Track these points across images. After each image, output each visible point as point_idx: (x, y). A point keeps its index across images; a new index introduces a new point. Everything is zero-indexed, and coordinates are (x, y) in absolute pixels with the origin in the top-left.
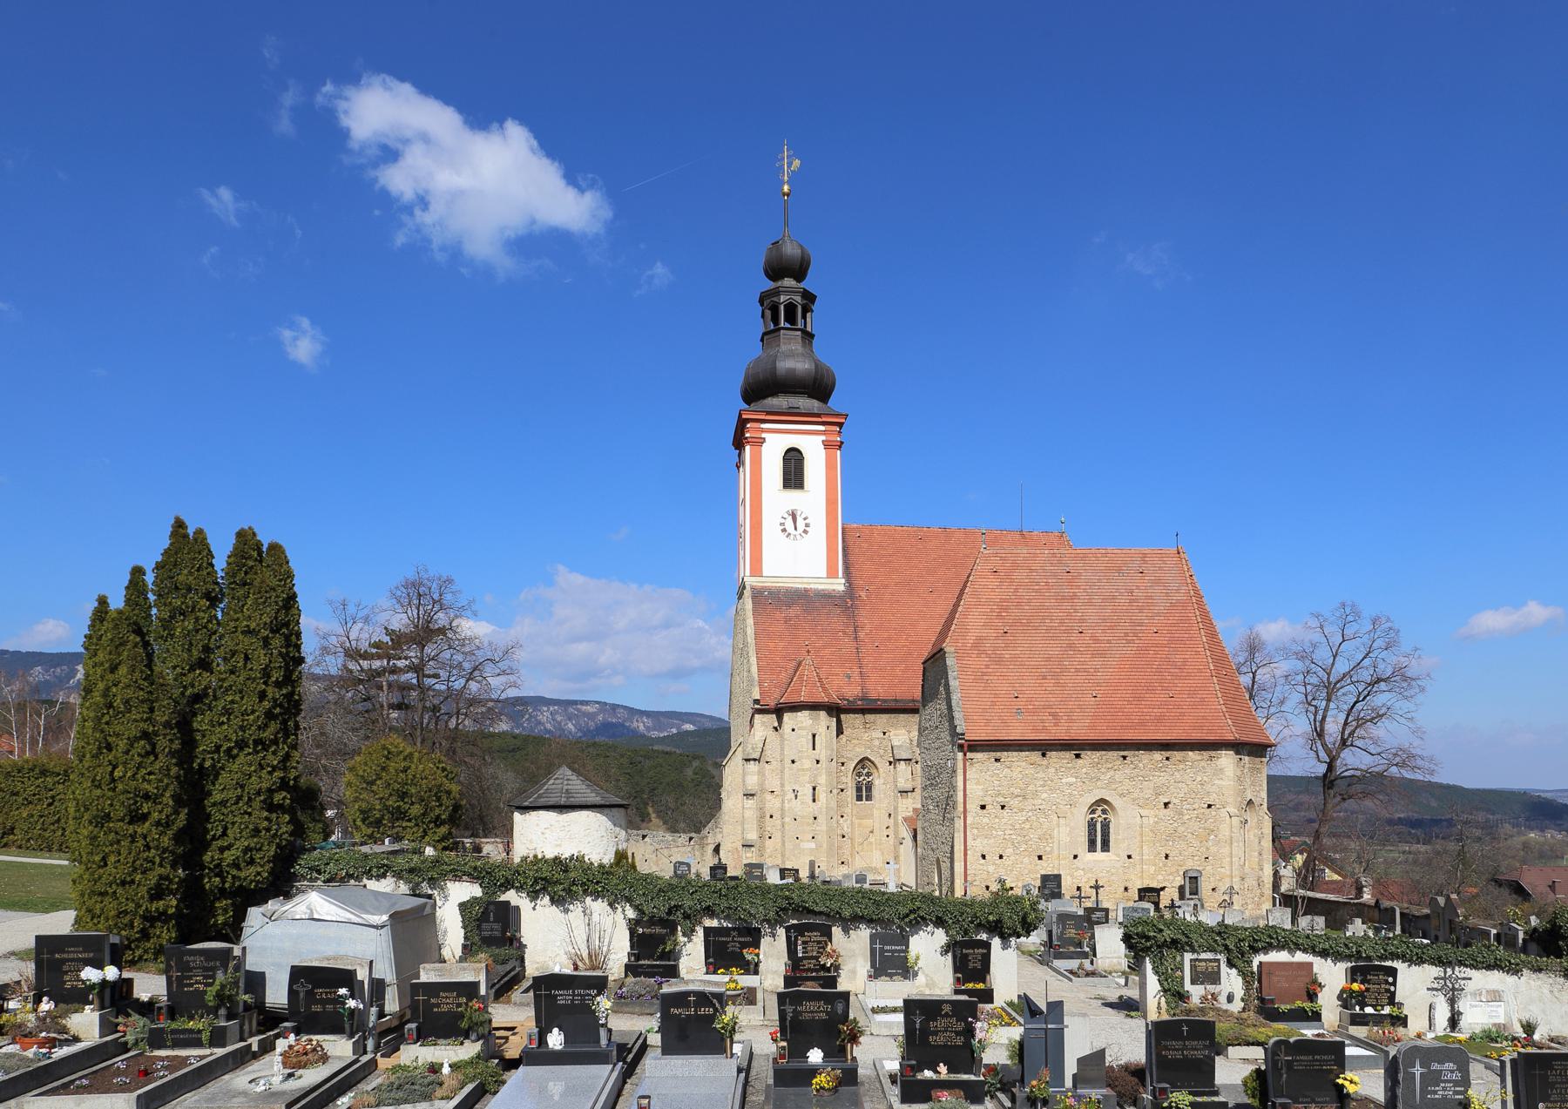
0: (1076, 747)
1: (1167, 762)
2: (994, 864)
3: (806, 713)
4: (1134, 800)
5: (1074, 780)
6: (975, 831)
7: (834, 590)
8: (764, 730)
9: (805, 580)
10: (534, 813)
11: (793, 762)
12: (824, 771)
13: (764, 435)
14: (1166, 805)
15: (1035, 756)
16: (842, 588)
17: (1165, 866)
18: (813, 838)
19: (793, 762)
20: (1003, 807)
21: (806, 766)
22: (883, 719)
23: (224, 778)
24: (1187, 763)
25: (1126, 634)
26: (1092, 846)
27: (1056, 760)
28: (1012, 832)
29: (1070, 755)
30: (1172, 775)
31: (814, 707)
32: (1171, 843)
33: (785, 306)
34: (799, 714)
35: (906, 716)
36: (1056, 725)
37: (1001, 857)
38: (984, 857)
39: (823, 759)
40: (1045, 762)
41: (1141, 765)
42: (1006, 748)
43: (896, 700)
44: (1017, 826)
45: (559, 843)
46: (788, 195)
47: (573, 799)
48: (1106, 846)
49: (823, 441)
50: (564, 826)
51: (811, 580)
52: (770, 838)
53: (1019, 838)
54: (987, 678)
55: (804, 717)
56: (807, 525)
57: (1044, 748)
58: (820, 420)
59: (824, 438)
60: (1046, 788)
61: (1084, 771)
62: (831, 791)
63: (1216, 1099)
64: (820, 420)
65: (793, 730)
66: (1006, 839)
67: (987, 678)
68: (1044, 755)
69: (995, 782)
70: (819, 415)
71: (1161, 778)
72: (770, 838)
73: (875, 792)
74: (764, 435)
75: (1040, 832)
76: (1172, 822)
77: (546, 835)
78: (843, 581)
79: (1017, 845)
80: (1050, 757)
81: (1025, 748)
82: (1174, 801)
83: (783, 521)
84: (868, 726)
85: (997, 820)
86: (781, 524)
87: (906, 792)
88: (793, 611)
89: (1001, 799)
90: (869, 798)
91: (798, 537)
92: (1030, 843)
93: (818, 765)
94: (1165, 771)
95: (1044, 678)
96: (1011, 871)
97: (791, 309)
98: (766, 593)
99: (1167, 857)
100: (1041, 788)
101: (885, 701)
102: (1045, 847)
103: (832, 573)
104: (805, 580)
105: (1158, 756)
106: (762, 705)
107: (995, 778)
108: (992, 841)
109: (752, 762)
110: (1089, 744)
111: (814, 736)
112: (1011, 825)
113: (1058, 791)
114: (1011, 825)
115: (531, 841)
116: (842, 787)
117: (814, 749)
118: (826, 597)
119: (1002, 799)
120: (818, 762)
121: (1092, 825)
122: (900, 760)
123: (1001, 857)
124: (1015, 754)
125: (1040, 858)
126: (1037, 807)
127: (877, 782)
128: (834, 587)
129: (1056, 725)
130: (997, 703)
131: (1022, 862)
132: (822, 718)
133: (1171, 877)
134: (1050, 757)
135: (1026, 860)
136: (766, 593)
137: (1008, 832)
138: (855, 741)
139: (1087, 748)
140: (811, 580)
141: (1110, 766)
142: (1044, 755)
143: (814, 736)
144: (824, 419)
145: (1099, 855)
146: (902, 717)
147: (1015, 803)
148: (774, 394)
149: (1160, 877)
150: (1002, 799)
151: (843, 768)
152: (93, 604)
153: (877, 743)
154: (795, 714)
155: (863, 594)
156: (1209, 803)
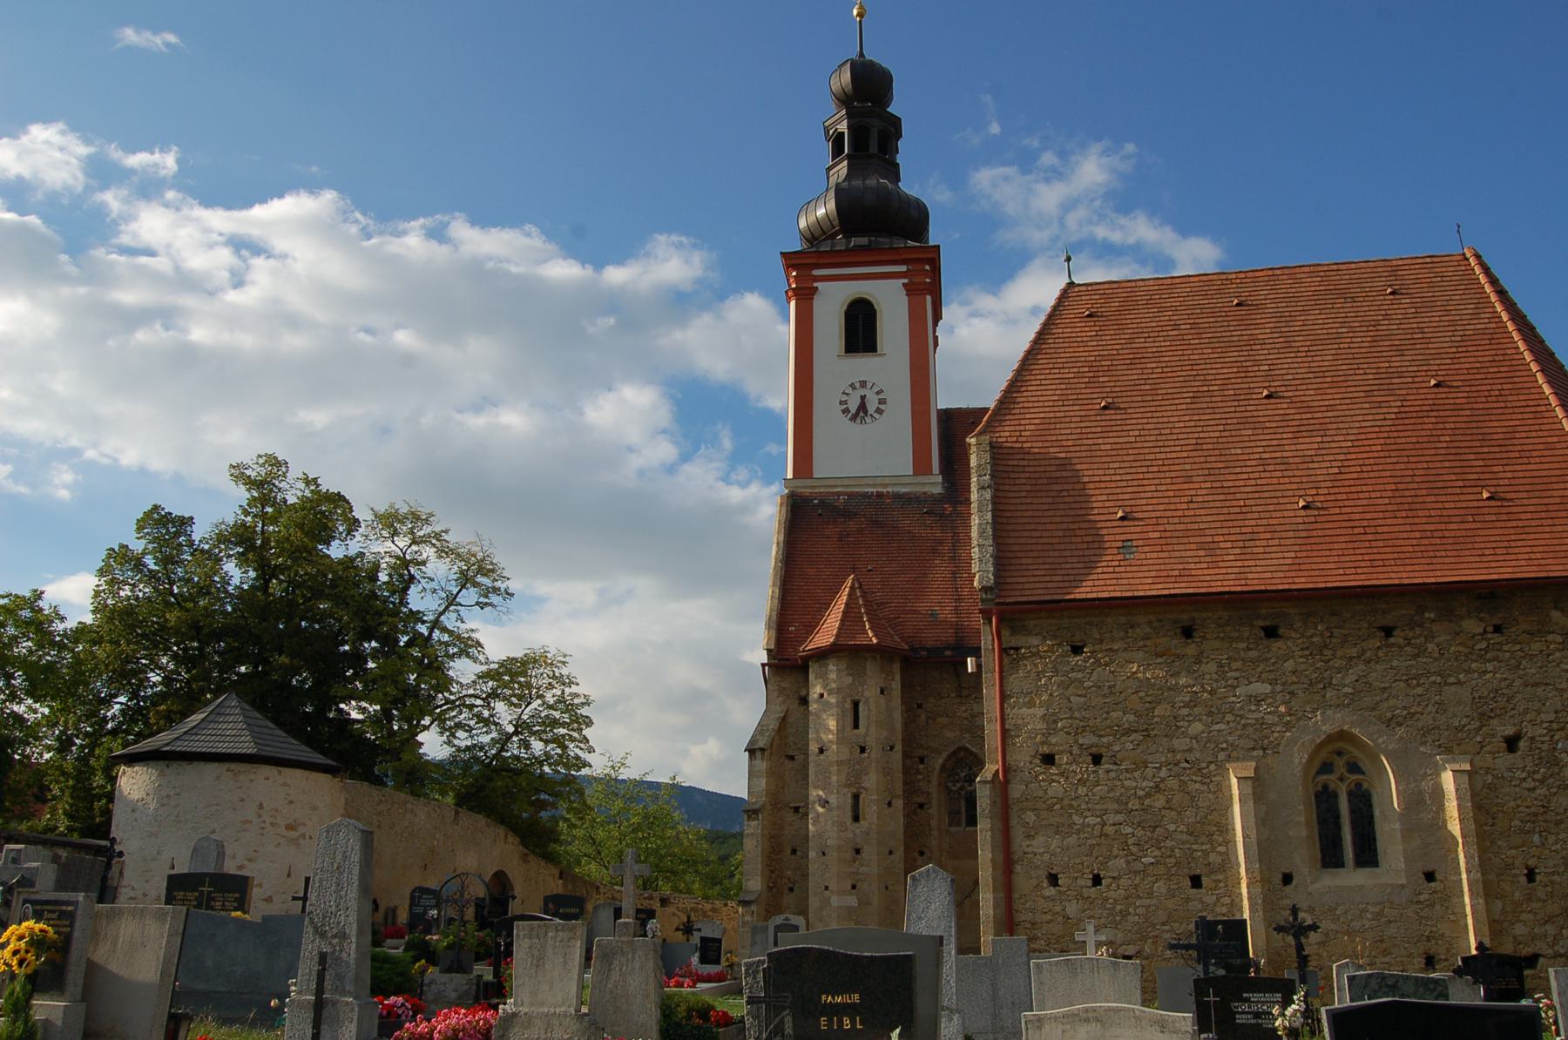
1: (1497, 638)
2: (1080, 897)
4: (1426, 731)
5: (1267, 688)
6: (1030, 817)
7: (925, 493)
8: (784, 702)
12: (874, 764)
13: (815, 285)
14: (1512, 743)
16: (938, 490)
17: (1529, 898)
18: (854, 887)
20: (1097, 759)
24: (1550, 637)
25: (1369, 394)
26: (1331, 857)
27: (1217, 644)
28: (1120, 818)
30: (1518, 667)
32: (1536, 838)
36: (1214, 564)
37: (1097, 880)
38: (1053, 880)
39: (870, 742)
40: (1191, 650)
41: (1431, 646)
44: (1134, 804)
48: (1367, 855)
52: (791, 890)
53: (1139, 832)
54: (1059, 487)
56: (882, 402)
61: (1289, 665)
62: (890, 804)
66: (1106, 835)
67: (1059, 487)
72: (791, 890)
74: (815, 285)
75: (1190, 816)
76: (1529, 784)
78: (940, 479)
79: (1134, 849)
80: (1204, 637)
83: (845, 398)
85: (1082, 791)
86: (841, 403)
89: (1087, 739)
92: (1169, 843)
94: (1496, 659)
95: (1188, 480)
96: (1125, 914)
98: (816, 502)
99: (1531, 875)
100: (1185, 711)
102: (1206, 854)
103: (921, 466)
107: (1071, 690)
108: (1072, 840)
111: (856, 705)
112: (1118, 800)
113: (1229, 717)
114: (1118, 800)
116: (921, 800)
117: (856, 726)
119: (1093, 739)
120: (863, 750)
121: (1325, 801)
123: (1097, 880)
125: (1196, 881)
128: (926, 489)
129: (1214, 564)
130: (1079, 533)
131: (1150, 894)
132: (869, 673)
133: (1551, 929)
134: (1204, 637)
135: (1160, 887)
136: (816, 502)
137: (1111, 818)
138: (943, 720)
141: (1354, 652)
143: (856, 705)
145: (1352, 878)
149: (1519, 930)
150: (1093, 739)
151: (921, 766)
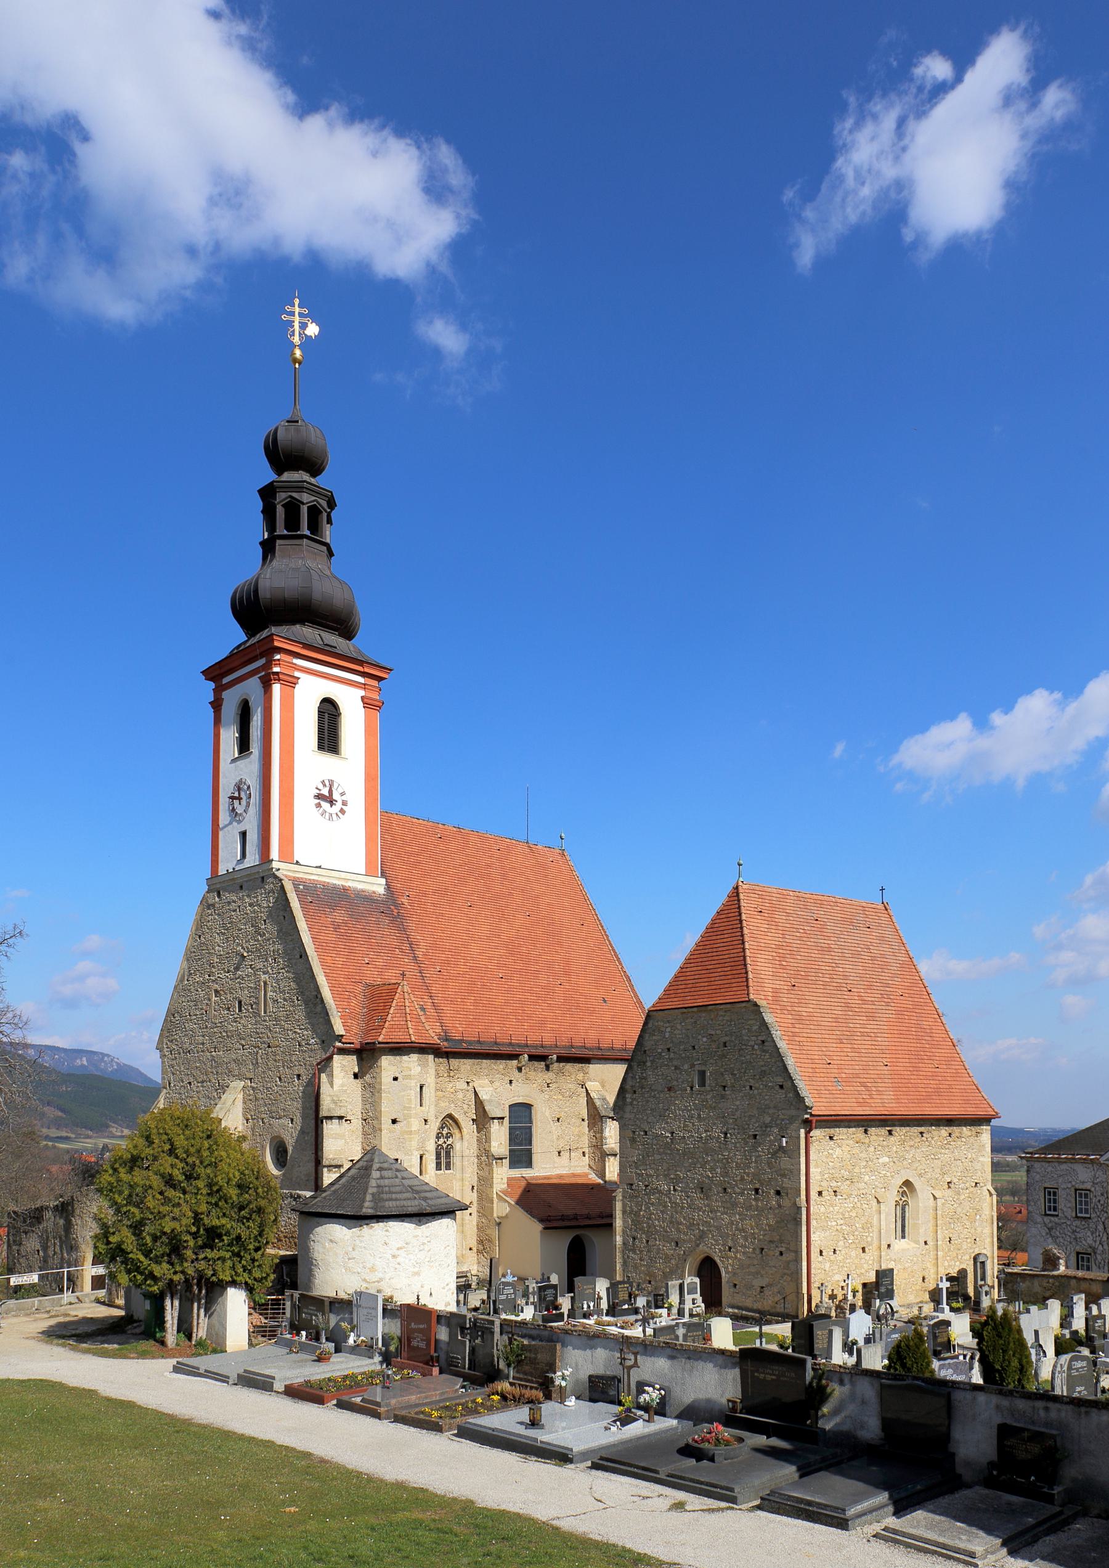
0: (888, 1122)
3: (414, 1057)
7: (374, 892)
9: (343, 875)
10: (379, 1228)
11: (394, 1121)
13: (297, 674)
15: (857, 1133)
19: (394, 1121)
21: (414, 1128)
22: (466, 1065)
23: (257, 1217)
29: (883, 1131)
31: (423, 1049)
33: (308, 507)
34: (405, 1058)
35: (488, 1061)
42: (838, 1124)
43: (511, 1044)
45: (416, 1270)
46: (300, 364)
47: (391, 1204)
49: (363, 698)
50: (424, 1244)
51: (348, 876)
55: (412, 1061)
57: (866, 1124)
58: (360, 668)
59: (362, 693)
60: (868, 1170)
63: (658, 1476)
64: (360, 668)
65: (395, 1079)
68: (866, 1132)
69: (830, 1164)
70: (361, 663)
71: (946, 1156)
73: (456, 1160)
77: (399, 1260)
79: (846, 1236)
81: (852, 1124)
82: (955, 1180)
84: (452, 1074)
87: (501, 1159)
88: (340, 916)
89: (834, 1184)
90: (448, 1167)
91: (334, 816)
93: (427, 1126)
97: (314, 512)
98: (301, 887)
101: (470, 1043)
104: (343, 875)
105: (944, 1131)
106: (343, 1043)
109: (335, 1121)
110: (899, 1120)
115: (373, 1269)
118: (367, 898)
122: (494, 1118)
124: (845, 1130)
126: (861, 1192)
127: (458, 1146)
135: (853, 1254)
139: (897, 1123)
140: (348, 876)
142: (866, 1132)
144: (367, 670)
146: (486, 1063)
147: (844, 1187)
148: (302, 622)
152: (718, 900)
153: (460, 1095)
154: (398, 1058)
155: (405, 901)
156: (976, 1181)
